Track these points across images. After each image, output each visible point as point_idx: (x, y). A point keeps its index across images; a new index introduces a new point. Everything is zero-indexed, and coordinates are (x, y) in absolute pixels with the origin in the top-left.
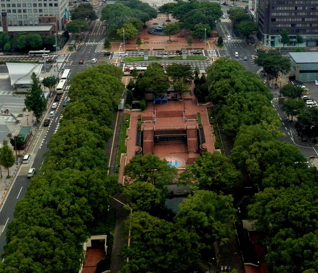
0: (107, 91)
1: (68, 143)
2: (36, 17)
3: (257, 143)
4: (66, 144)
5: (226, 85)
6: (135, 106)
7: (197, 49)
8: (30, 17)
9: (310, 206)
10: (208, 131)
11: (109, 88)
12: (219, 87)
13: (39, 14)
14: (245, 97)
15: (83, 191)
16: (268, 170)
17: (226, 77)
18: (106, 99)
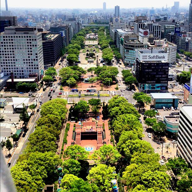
0: (59, 112)
1: (38, 138)
2: (28, 74)
3: (130, 140)
4: (37, 139)
5: (117, 110)
6: (73, 120)
7: (91, 95)
8: (25, 74)
9: (152, 174)
10: (108, 132)
11: (60, 111)
12: (113, 111)
13: (29, 72)
14: (126, 117)
15: (42, 162)
16: (134, 155)
17: (118, 106)
18: (57, 116)
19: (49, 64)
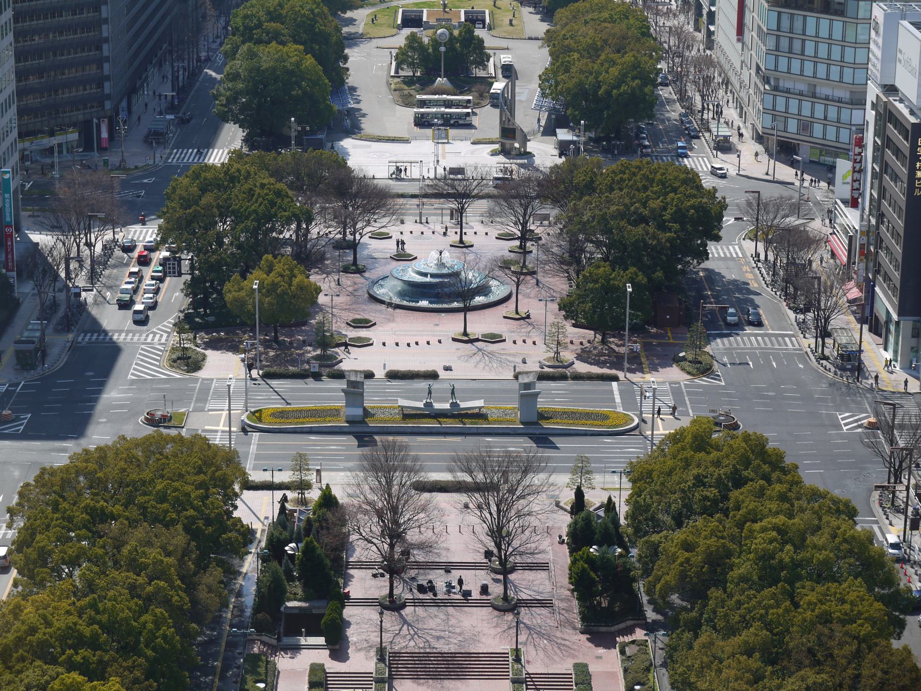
19: (63, 129)
